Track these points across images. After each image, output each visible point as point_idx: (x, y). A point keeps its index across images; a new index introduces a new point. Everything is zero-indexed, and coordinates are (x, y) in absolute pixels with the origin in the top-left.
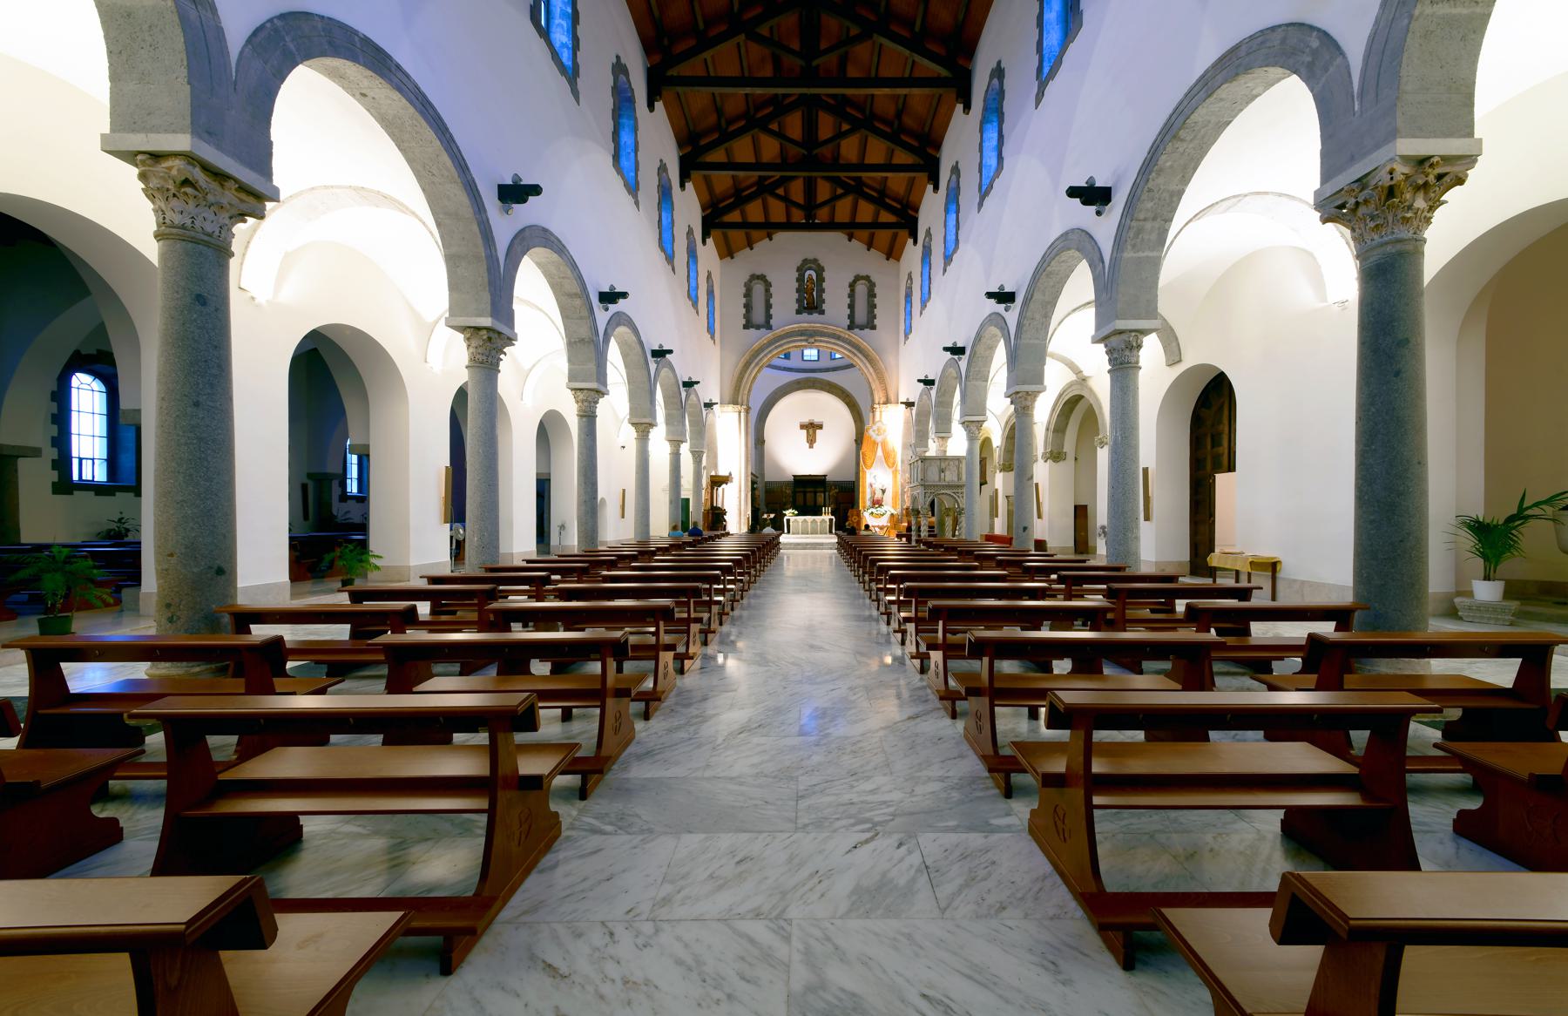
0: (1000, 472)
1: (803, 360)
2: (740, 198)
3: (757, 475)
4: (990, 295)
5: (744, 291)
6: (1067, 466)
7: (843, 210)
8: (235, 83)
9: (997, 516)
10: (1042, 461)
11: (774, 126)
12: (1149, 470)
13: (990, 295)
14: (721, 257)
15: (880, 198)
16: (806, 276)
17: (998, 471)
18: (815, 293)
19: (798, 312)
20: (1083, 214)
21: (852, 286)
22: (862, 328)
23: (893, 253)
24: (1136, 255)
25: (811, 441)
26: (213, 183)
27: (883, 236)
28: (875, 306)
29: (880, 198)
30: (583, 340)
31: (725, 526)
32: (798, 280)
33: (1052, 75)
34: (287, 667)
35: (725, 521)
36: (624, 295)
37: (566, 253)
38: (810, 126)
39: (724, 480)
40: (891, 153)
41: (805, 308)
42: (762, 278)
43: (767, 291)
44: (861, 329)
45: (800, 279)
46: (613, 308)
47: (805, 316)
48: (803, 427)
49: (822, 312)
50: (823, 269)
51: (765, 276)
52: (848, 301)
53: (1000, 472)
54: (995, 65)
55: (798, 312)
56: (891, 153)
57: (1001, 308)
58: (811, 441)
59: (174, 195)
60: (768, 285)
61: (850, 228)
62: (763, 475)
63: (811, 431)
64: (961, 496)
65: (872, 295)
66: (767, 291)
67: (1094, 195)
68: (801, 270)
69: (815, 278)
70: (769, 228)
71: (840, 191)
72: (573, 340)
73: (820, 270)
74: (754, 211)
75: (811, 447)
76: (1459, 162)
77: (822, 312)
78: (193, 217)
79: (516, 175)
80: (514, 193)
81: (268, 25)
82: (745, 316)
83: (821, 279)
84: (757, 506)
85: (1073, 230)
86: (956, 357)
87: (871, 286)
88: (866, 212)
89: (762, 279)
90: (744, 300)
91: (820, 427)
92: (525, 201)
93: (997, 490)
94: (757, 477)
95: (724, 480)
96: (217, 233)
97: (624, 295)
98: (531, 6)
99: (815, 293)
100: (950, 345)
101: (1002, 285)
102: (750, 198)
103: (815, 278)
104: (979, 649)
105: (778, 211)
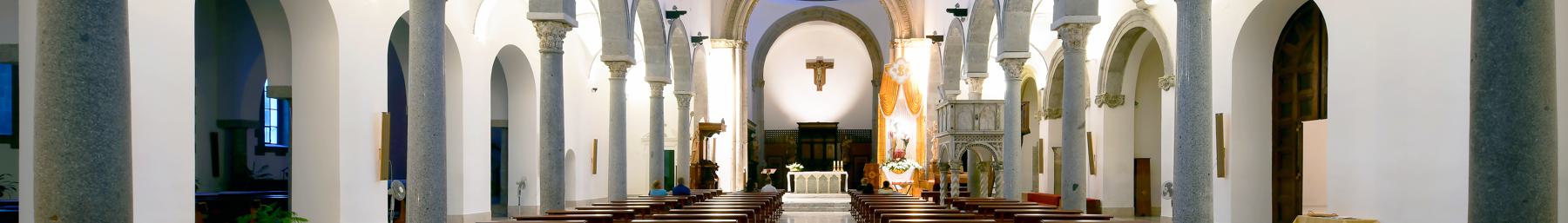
0: (1046, 118)
6: (1127, 110)
9: (1042, 172)
17: (1043, 118)
25: (820, 82)
31: (717, 183)
35: (717, 177)
48: (809, 65)
53: (1046, 118)
58: (820, 82)
62: (762, 122)
91: (831, 65)
93: (1041, 141)
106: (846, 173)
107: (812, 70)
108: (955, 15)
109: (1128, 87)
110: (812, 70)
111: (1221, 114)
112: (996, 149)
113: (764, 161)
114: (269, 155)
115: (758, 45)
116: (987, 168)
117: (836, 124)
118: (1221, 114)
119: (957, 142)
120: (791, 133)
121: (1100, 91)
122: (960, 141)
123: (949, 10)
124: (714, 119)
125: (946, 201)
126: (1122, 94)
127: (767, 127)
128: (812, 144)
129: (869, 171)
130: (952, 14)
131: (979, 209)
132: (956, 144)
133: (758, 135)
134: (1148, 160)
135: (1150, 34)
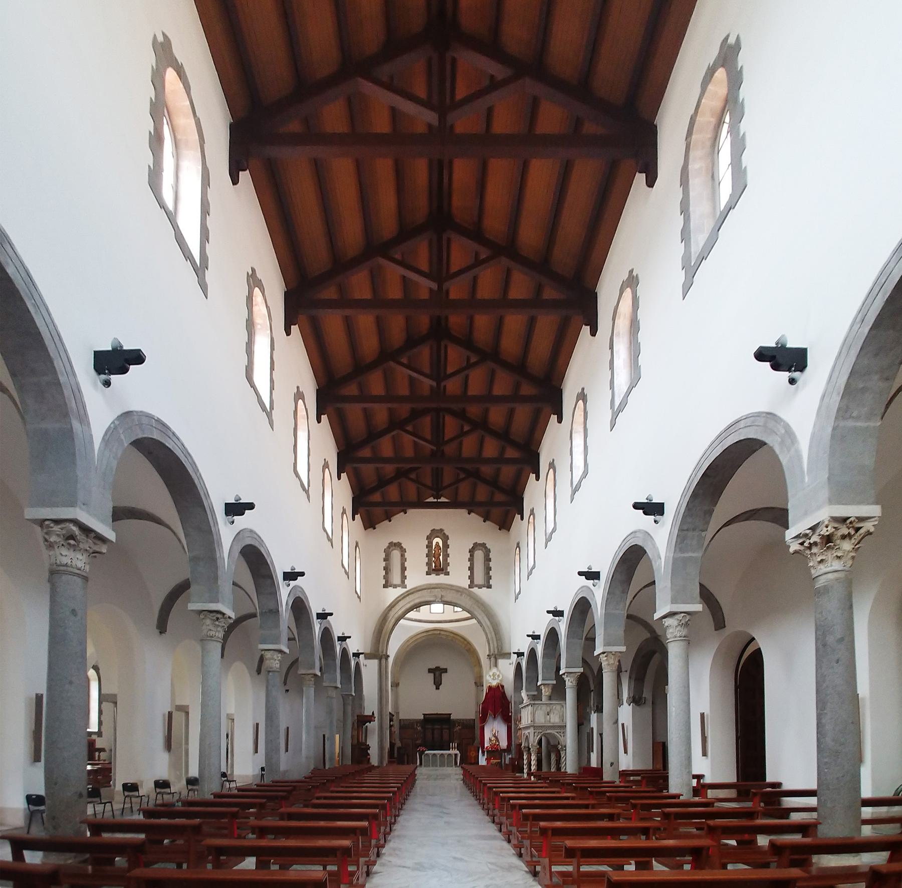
0: (595, 713)
1: (430, 612)
2: (382, 483)
3: (393, 713)
4: (581, 574)
5: (384, 556)
6: (647, 710)
7: (464, 490)
8: (96, 467)
9: (593, 751)
10: (627, 705)
11: (409, 428)
12: (705, 714)
13: (581, 574)
14: (366, 528)
15: (494, 483)
16: (434, 544)
17: (593, 712)
18: (441, 557)
19: (428, 573)
20: (645, 521)
21: (472, 551)
22: (480, 587)
23: (505, 525)
24: (682, 555)
25: (438, 684)
26: (83, 535)
27: (496, 511)
28: (490, 569)
29: (494, 483)
30: (272, 610)
31: (369, 759)
32: (427, 547)
33: (621, 408)
34: (116, 859)
35: (369, 755)
36: (302, 574)
37: (264, 545)
38: (438, 428)
39: (370, 719)
40: (503, 450)
41: (433, 570)
42: (398, 545)
43: (402, 556)
44: (479, 588)
45: (429, 546)
46: (292, 583)
47: (433, 575)
48: (430, 671)
49: (447, 574)
50: (447, 538)
51: (401, 544)
52: (468, 564)
53: (595, 713)
54: (580, 391)
55: (428, 573)
56: (503, 450)
57: (590, 583)
58: (438, 684)
59: (62, 545)
60: (403, 551)
61: (471, 506)
62: (398, 713)
63: (437, 673)
64: (562, 735)
65: (487, 559)
66: (402, 556)
67: (653, 509)
68: (430, 538)
69: (441, 545)
70: (404, 505)
71: (462, 476)
72: (264, 611)
73: (445, 538)
74: (393, 492)
75: (437, 688)
76: (869, 520)
77: (447, 574)
78: (71, 559)
79: (237, 495)
80: (236, 509)
81: (112, 426)
82: (385, 577)
83: (446, 546)
84: (393, 742)
85: (640, 531)
86: (557, 618)
87: (487, 552)
88: (482, 492)
89: (402, 551)
90: (384, 564)
91: (445, 670)
92: (243, 514)
93: (592, 728)
94: (393, 716)
95: (370, 719)
96: (83, 568)
97: (302, 574)
98: (246, 366)
99: (441, 557)
100: (553, 609)
101: (590, 566)
102: (390, 481)
103: (441, 545)
104: (571, 853)
105: (412, 490)
106: (458, 752)
107: (432, 675)
108: (532, 639)
109: (647, 694)
110: (432, 675)
111: (704, 713)
112: (561, 735)
113: (399, 742)
114: (103, 729)
115: (395, 657)
116: (383, 657)
117: (450, 714)
118: (704, 713)
119: (535, 731)
120: (417, 722)
121: (629, 694)
122: (538, 731)
123: (528, 636)
124: (368, 712)
125: (528, 774)
126: (643, 696)
127: (402, 717)
128: (433, 730)
129: (470, 751)
130: (530, 638)
131: (550, 781)
132: (534, 733)
133: (395, 723)
134: (703, 756)
135: (757, 644)
